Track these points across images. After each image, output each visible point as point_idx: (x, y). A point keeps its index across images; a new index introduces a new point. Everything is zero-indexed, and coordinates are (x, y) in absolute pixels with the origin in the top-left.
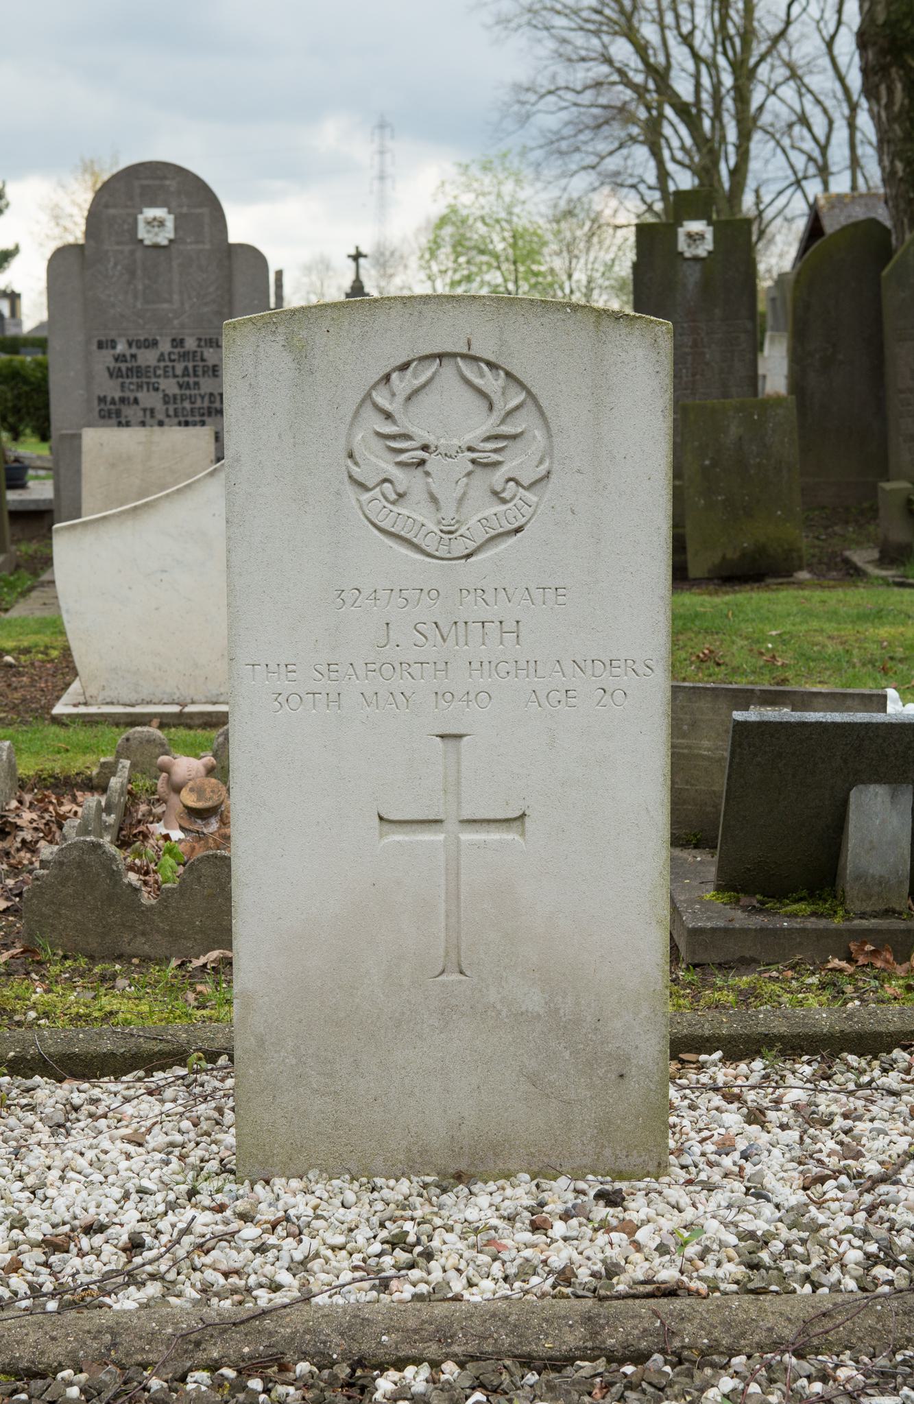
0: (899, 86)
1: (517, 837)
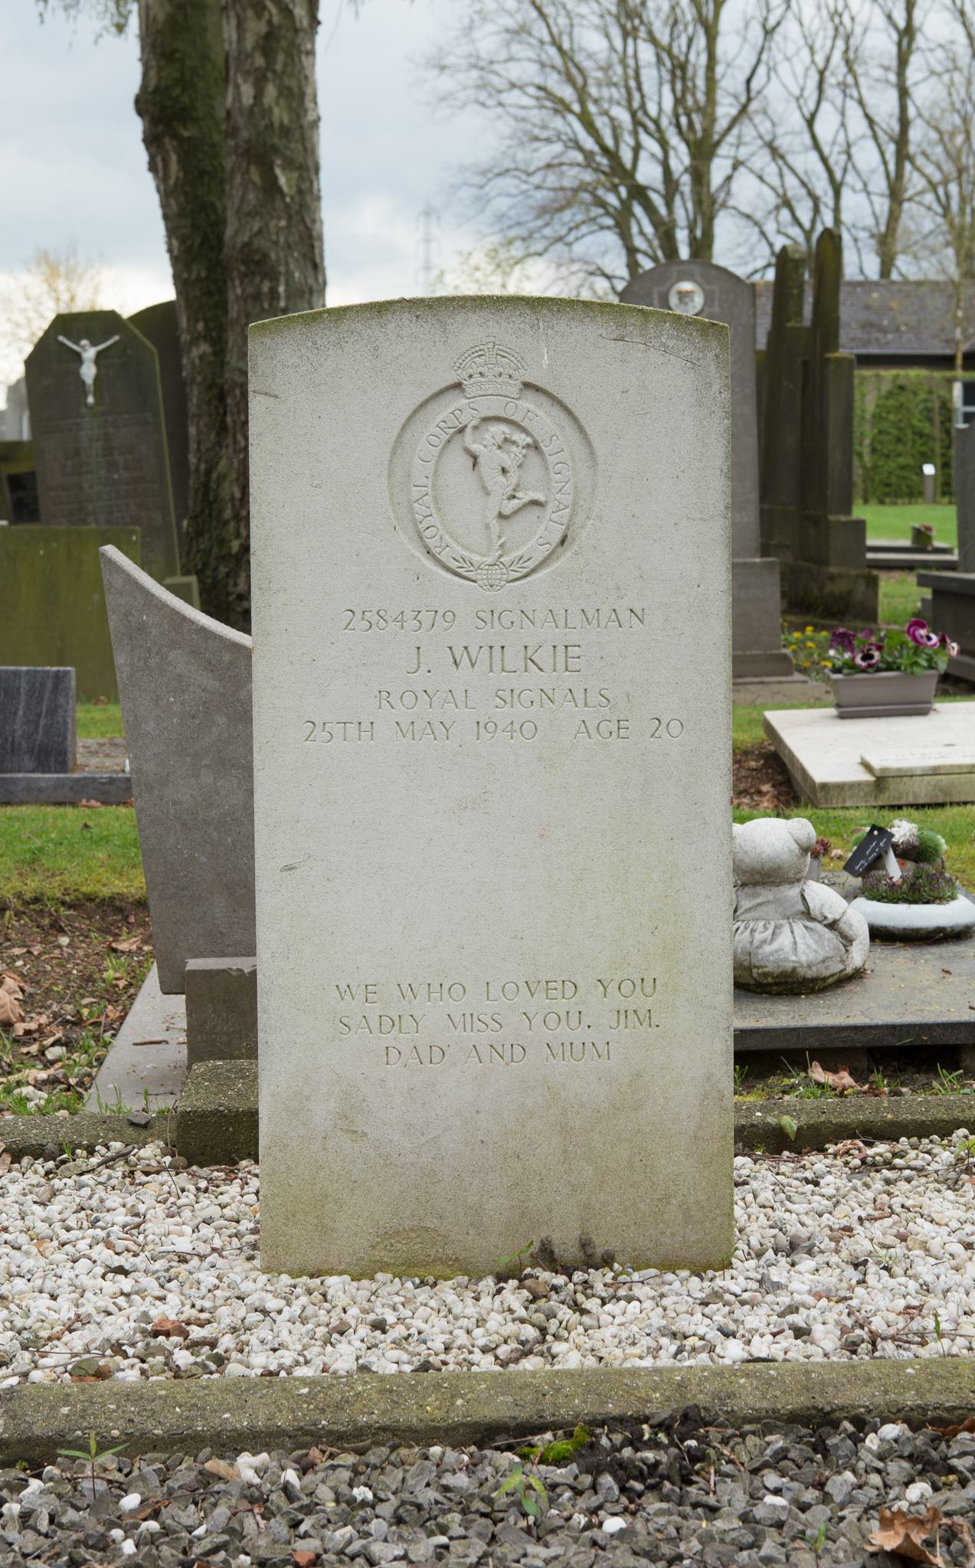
0: (174, 157)
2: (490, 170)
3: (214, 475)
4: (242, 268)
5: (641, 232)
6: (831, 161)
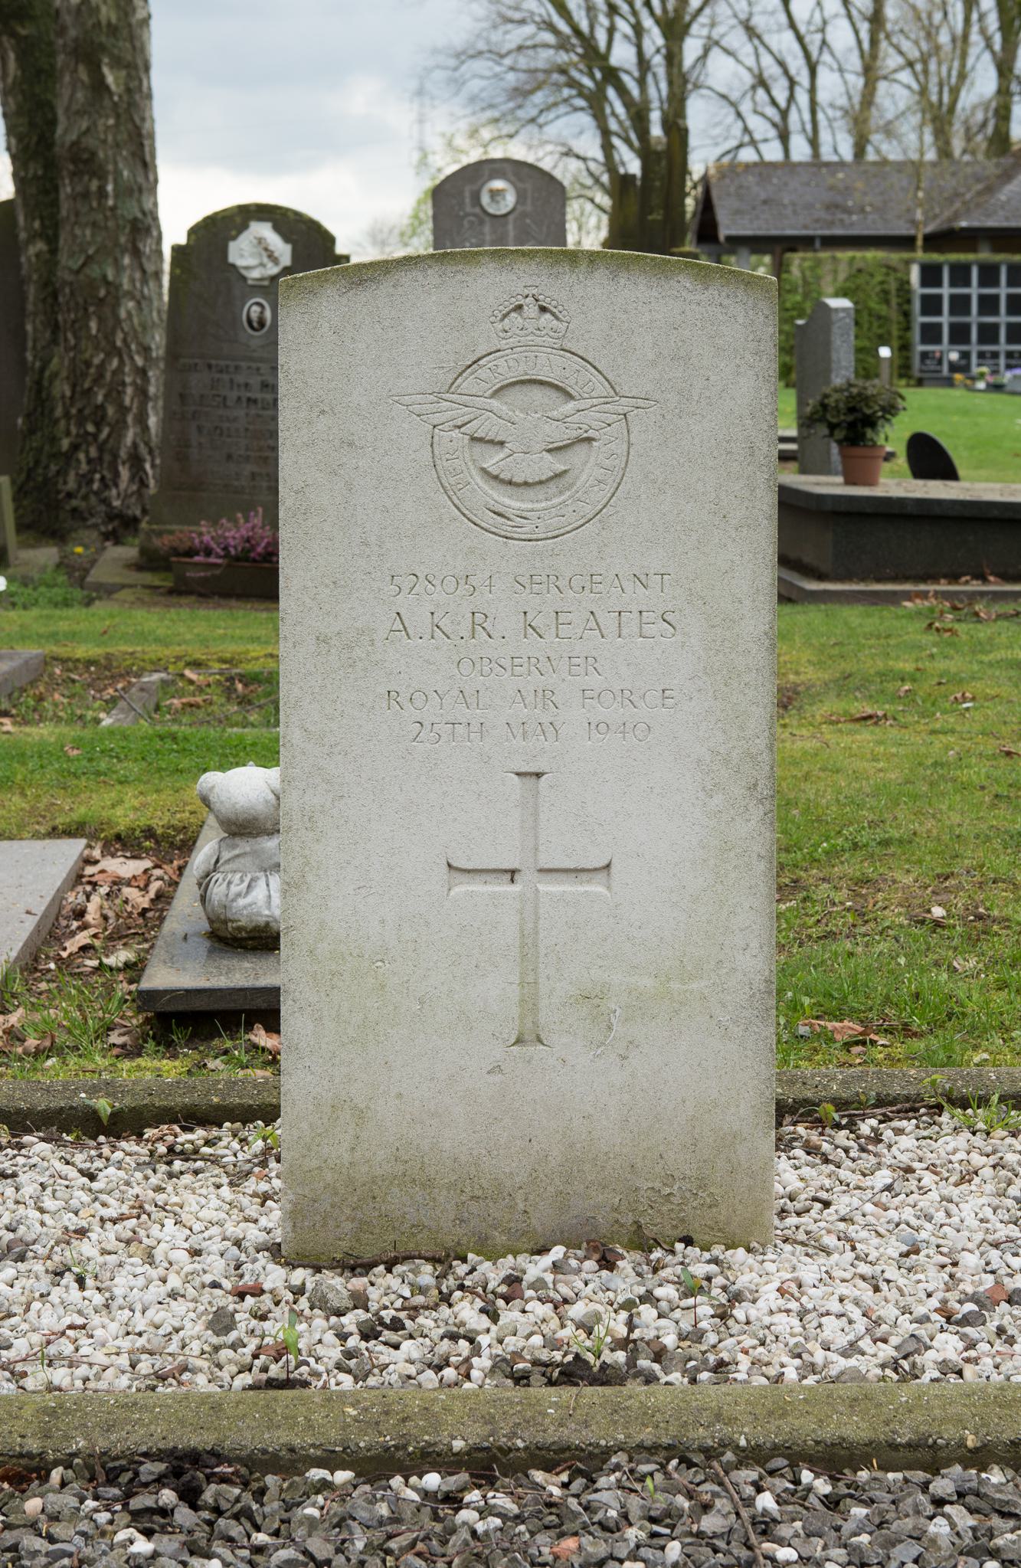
0: (12, 56)
1: (601, 889)
2: (463, 52)
3: (47, 374)
4: (71, 167)
5: (614, 114)
6: (807, 39)
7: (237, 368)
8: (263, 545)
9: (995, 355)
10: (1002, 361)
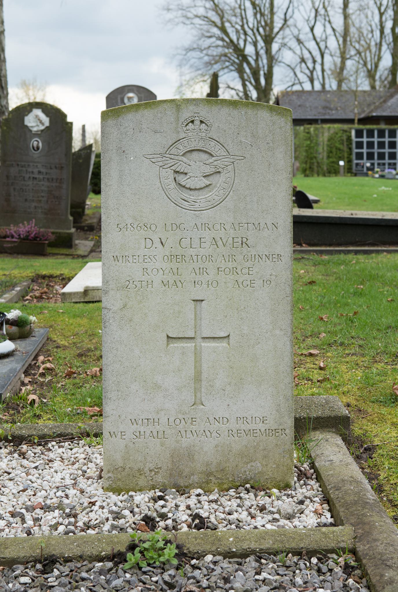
7: (29, 165)
8: (34, 234)
9: (384, 164)
10: (387, 166)
